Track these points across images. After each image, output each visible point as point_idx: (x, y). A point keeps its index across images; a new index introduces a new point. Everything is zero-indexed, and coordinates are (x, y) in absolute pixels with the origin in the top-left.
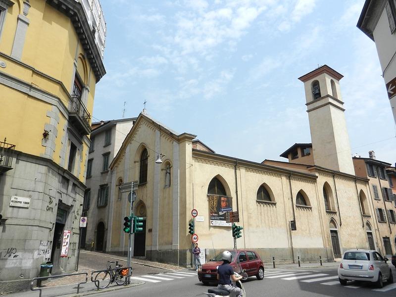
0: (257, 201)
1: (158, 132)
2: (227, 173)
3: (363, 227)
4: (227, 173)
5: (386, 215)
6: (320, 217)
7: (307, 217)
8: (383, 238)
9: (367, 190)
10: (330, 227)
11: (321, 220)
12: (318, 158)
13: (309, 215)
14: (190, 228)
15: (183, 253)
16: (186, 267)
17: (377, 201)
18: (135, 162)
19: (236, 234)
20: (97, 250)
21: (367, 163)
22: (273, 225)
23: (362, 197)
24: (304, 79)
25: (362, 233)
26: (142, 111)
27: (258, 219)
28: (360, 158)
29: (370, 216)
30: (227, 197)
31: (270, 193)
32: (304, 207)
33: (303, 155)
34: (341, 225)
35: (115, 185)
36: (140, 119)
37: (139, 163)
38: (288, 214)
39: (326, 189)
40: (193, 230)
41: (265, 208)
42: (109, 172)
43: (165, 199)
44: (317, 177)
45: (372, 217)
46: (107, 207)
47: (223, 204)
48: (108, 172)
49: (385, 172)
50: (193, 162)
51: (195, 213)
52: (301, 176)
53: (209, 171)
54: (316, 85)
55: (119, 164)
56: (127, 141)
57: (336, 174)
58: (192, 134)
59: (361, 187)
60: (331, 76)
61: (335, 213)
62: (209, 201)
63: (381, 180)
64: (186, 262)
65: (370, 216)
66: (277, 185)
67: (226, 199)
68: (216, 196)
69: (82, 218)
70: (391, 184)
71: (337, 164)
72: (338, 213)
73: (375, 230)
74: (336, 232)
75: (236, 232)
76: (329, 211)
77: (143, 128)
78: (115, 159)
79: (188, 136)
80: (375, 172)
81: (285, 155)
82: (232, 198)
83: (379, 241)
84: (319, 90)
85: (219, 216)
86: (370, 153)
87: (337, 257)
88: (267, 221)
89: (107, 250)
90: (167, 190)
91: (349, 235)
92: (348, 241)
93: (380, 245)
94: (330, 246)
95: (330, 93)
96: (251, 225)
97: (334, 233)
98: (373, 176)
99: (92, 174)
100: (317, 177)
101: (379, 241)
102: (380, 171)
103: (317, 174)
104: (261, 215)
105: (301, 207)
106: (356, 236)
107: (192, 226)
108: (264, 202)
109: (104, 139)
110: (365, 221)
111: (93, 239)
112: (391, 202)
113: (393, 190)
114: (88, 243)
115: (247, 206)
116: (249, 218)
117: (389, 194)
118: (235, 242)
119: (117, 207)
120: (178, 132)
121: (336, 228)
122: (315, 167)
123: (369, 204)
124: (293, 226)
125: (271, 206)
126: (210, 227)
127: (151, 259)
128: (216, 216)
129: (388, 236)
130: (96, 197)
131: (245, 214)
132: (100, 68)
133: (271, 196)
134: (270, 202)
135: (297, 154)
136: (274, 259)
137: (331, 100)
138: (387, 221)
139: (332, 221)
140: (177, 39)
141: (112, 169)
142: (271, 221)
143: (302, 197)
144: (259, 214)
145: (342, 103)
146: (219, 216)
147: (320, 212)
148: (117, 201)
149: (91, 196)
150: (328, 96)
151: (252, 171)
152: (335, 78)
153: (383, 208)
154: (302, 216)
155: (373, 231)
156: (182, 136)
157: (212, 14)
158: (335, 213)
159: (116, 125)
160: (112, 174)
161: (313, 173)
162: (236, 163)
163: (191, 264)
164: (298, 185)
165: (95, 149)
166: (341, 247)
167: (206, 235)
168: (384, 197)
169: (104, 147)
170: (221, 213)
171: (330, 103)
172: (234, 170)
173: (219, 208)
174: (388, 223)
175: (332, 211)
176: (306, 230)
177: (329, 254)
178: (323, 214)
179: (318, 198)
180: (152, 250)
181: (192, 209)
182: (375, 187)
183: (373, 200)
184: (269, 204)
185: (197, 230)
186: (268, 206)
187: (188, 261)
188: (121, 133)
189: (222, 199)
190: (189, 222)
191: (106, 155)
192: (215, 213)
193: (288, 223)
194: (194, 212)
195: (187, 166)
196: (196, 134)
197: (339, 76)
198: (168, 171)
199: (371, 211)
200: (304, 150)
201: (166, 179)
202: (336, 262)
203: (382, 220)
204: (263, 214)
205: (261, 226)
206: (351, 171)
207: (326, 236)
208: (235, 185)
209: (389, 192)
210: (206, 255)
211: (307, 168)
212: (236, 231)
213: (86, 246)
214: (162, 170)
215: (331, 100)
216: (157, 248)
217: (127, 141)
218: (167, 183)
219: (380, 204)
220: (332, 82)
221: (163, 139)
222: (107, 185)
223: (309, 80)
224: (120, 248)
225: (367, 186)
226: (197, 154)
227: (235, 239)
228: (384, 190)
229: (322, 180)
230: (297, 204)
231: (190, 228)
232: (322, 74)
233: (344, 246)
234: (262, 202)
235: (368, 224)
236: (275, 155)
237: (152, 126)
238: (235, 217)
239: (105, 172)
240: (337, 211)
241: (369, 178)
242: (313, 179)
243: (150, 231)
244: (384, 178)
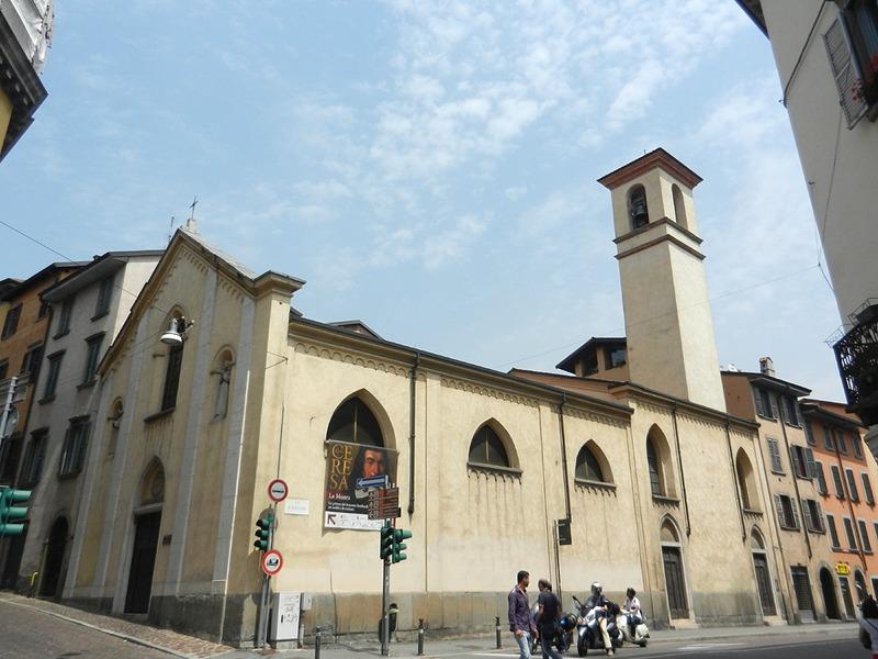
0: (469, 466)
1: (212, 275)
2: (388, 389)
3: (744, 539)
4: (388, 389)
5: (799, 515)
6: (638, 512)
7: (604, 508)
8: (792, 567)
9: (755, 451)
10: (663, 539)
11: (639, 520)
12: (639, 370)
13: (607, 506)
14: (258, 533)
15: (236, 606)
16: (237, 647)
17: (777, 477)
18: (155, 356)
19: (390, 552)
20: (45, 595)
21: (754, 384)
22: (511, 532)
23: (742, 465)
24: (611, 181)
25: (742, 555)
26: (185, 225)
27: (469, 514)
28: (740, 374)
29: (761, 515)
30: (385, 453)
31: (508, 448)
32: (597, 485)
33: (609, 366)
34: (689, 534)
35: (105, 418)
36: (178, 243)
37: (167, 357)
38: (551, 501)
39: (655, 443)
40: (265, 538)
41: (490, 485)
42: (96, 386)
43: (210, 451)
44: (632, 411)
45: (765, 515)
46: (80, 478)
47: (370, 469)
48: (92, 384)
49: (797, 408)
50: (290, 351)
51: (279, 490)
52: (591, 407)
53: (339, 378)
54: (638, 196)
55: (119, 363)
56: (144, 301)
57: (680, 407)
58: (293, 275)
59: (739, 441)
60: (675, 177)
61: (676, 503)
62: (329, 458)
63: (786, 427)
64: (239, 633)
65: (761, 515)
66: (525, 424)
67: (379, 455)
68: (350, 446)
70: (811, 438)
71: (684, 385)
72: (681, 505)
73: (774, 548)
74: (676, 551)
75: (391, 546)
76: (662, 498)
77: (184, 268)
78: (113, 350)
79: (279, 280)
80: (774, 406)
81: (561, 366)
82: (396, 454)
83: (782, 576)
84: (646, 208)
85: (354, 500)
86: (763, 363)
87: (677, 616)
88: (494, 520)
89: (65, 595)
90: (219, 425)
91: (708, 558)
92: (708, 574)
93: (784, 586)
94: (659, 587)
95: (670, 213)
96: (447, 528)
97: (672, 555)
98: (769, 416)
99: (59, 390)
100: (632, 411)
101: (782, 576)
102: (785, 405)
103: (632, 405)
104: (478, 501)
105: (587, 485)
106: (726, 562)
107: (266, 526)
108: (488, 469)
109: (95, 304)
110: (749, 525)
111: (37, 563)
112: (811, 481)
113: (814, 453)
114: (24, 575)
115: (440, 476)
116: (444, 508)
117: (807, 462)
118: (386, 573)
120: (252, 271)
121: (677, 540)
122: (627, 387)
123: (758, 485)
124: (564, 533)
125: (508, 480)
126: (325, 530)
127: (157, 622)
128: (344, 501)
129: (804, 565)
130: (59, 448)
131: (433, 499)
132: (23, 74)
133: (510, 453)
134: (504, 468)
135: (595, 364)
136: (498, 624)
137: (670, 231)
138: (801, 525)
139: (668, 523)
140: (376, 152)
141: (102, 375)
142: (506, 519)
143: (592, 463)
144: (473, 498)
145: (699, 241)
146: (354, 500)
147: (636, 496)
148: (105, 461)
149: (49, 448)
150: (666, 221)
151: (461, 386)
152: (682, 183)
153: (792, 495)
154: (589, 508)
155: (768, 551)
156: (263, 282)
157: (451, 108)
158: (676, 503)
159: (125, 263)
160: (101, 389)
161: (621, 402)
162: (416, 363)
163: (255, 639)
164: (582, 430)
165: (71, 327)
166: (688, 591)
167: (309, 554)
168: (793, 468)
169: (93, 320)
170: (360, 494)
171: (669, 238)
172: (409, 380)
173: (357, 471)
174: (802, 531)
175: (667, 497)
176: (600, 545)
178: (643, 506)
179: (632, 462)
181: (275, 478)
182: (773, 445)
183: (769, 473)
184: (501, 473)
185: (282, 539)
186: (499, 478)
187: (247, 629)
188: (136, 277)
189: (369, 454)
190: (263, 514)
191: (95, 340)
192: (344, 492)
193: (551, 524)
194: (277, 486)
195: (271, 359)
196: (302, 279)
197: (691, 179)
198: (225, 376)
199: (764, 501)
200: (613, 354)
201: (218, 397)
202: (673, 628)
203: (789, 523)
204: (483, 499)
205: (476, 532)
206: (715, 400)
207: (650, 561)
208: (408, 420)
209: (805, 454)
210: (301, 612)
211: (609, 388)
212: (390, 542)
213: (18, 583)
214: (212, 373)
215: (670, 231)
216: (177, 591)
217: (144, 301)
218: (221, 408)
219: (786, 486)
220: (675, 190)
221: (223, 293)
222: (88, 417)
225: (755, 440)
226: (304, 332)
227: (386, 565)
228: (795, 450)
229: (643, 418)
230: (577, 475)
231: (258, 533)
232: (651, 169)
233: (696, 589)
234: (483, 470)
235: (757, 534)
236: (546, 360)
237: (202, 261)
238: (387, 505)
239: (86, 385)
240: (679, 497)
241: (758, 420)
242: (622, 417)
243: (167, 540)
244: (794, 423)
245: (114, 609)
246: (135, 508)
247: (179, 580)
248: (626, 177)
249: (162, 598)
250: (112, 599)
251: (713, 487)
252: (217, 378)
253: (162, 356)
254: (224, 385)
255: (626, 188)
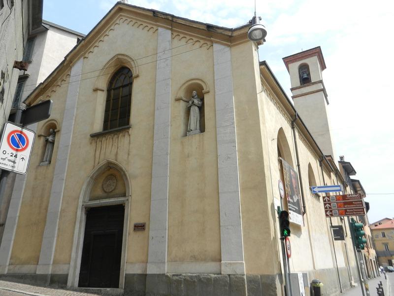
18: (96, 90)
69: (10, 127)
78: (42, 87)
84: (309, 74)
119: (36, 179)
177: (344, 278)
180: (148, 272)
216: (167, 269)
223: (296, 61)
224: (39, 267)
245: (69, 284)
246: (84, 202)
247: (166, 261)
248: (298, 58)
249: (144, 277)
250: (67, 275)
251: (160, 242)
252: (42, 139)
253: (103, 91)
254: (49, 146)
255: (295, 66)
